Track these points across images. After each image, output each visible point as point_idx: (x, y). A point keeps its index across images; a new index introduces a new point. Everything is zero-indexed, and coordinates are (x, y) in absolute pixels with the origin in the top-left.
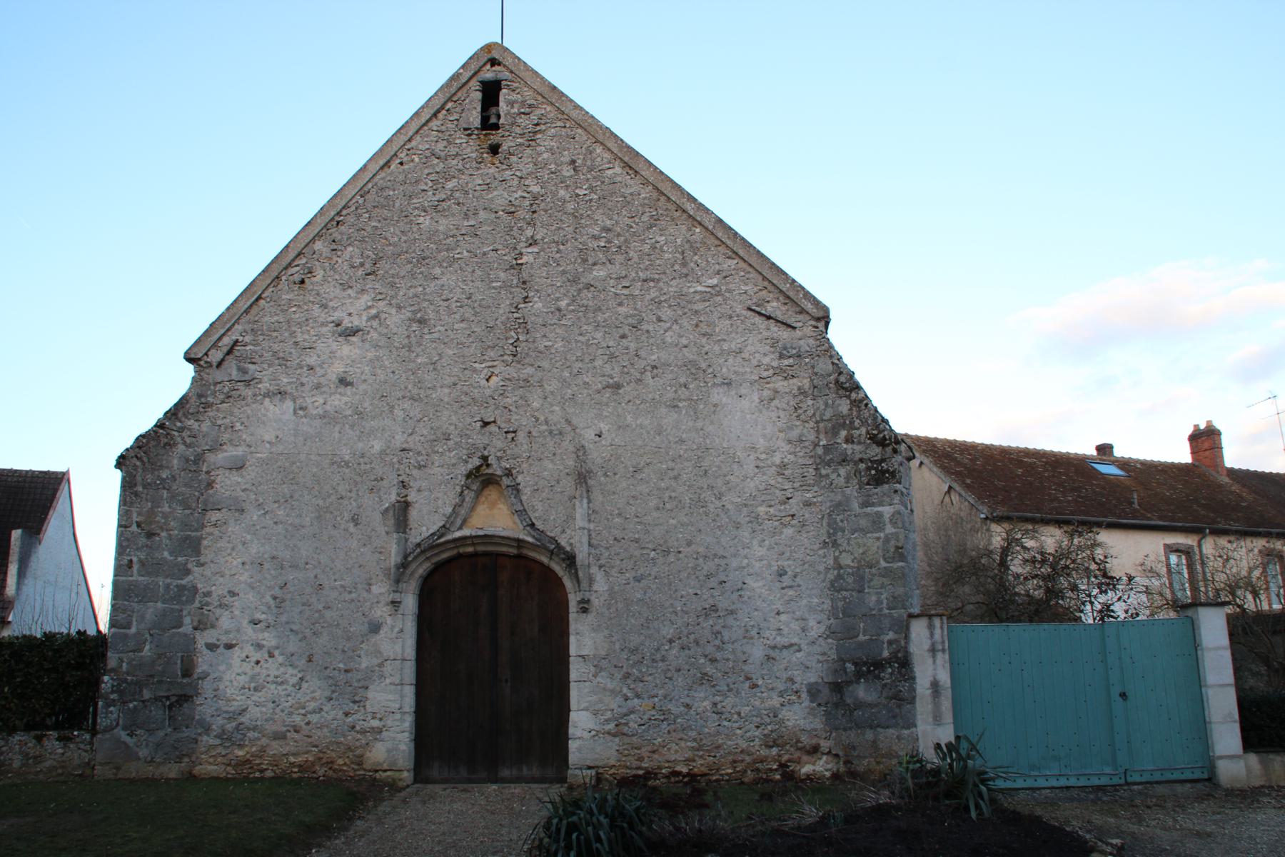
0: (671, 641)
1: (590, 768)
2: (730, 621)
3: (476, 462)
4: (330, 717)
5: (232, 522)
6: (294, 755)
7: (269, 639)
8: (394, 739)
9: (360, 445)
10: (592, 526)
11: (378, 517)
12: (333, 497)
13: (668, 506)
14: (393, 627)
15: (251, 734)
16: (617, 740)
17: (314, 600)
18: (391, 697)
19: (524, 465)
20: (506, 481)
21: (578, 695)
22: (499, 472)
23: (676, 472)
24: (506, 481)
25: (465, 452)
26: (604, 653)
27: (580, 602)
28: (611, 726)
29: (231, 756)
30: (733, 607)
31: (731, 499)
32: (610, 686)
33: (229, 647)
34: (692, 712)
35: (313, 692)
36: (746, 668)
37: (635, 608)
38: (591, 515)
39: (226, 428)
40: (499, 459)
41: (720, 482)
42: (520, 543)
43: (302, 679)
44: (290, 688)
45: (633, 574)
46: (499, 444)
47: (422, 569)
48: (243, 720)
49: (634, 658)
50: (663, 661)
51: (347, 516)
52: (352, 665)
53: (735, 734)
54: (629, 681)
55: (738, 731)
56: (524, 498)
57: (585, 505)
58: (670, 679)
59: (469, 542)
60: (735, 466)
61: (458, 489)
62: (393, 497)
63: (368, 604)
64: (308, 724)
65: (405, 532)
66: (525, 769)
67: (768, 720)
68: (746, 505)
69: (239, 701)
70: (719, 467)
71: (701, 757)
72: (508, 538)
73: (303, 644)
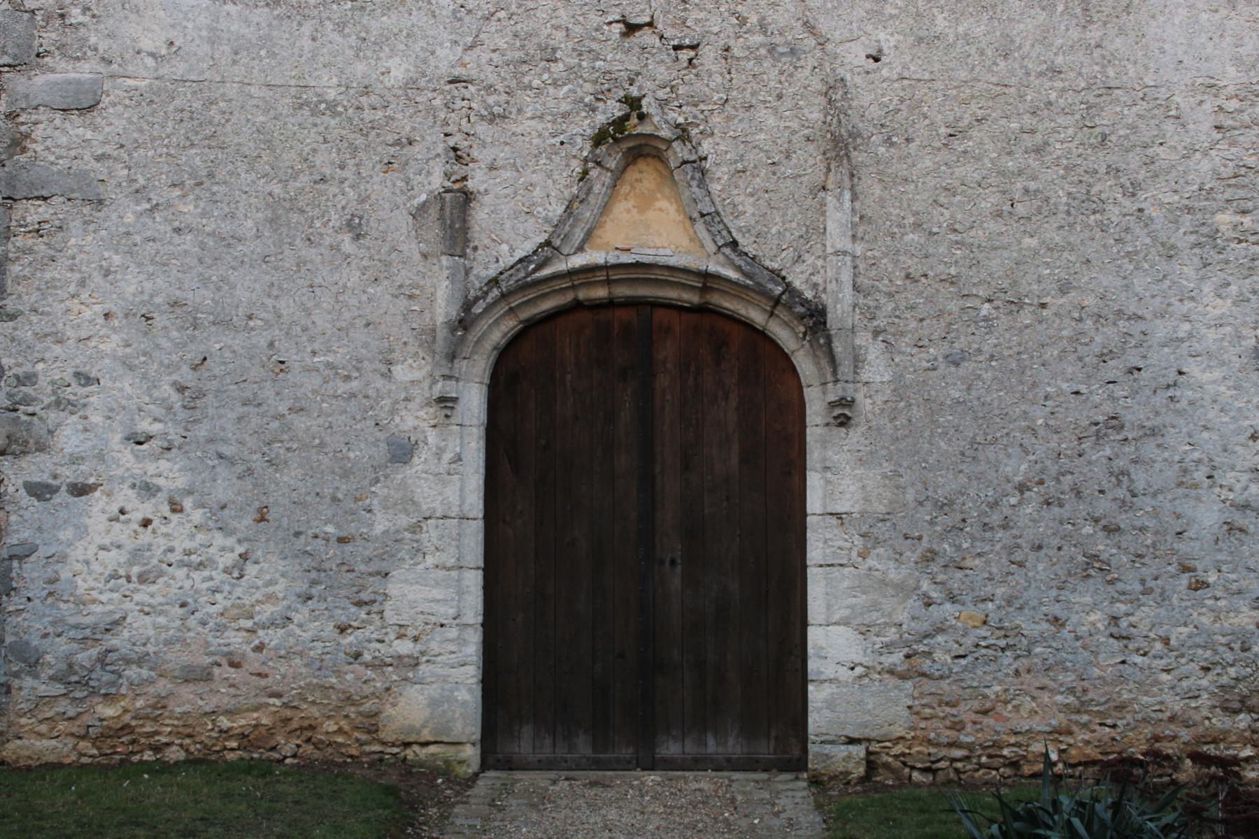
0: (1022, 488)
1: (851, 741)
2: (1149, 448)
3: (615, 109)
4: (307, 636)
5: (75, 225)
6: (229, 713)
7: (171, 474)
8: (445, 679)
9: (360, 68)
10: (859, 249)
11: (403, 222)
12: (304, 179)
13: (1020, 209)
14: (438, 455)
15: (132, 672)
16: (909, 685)
17: (268, 392)
18: (437, 593)
19: (716, 119)
20: (680, 151)
21: (823, 594)
22: (665, 133)
23: (1038, 138)
24: (680, 151)
25: (588, 87)
26: (882, 509)
27: (832, 405)
28: (896, 658)
29: (87, 719)
30: (1157, 421)
31: (1158, 197)
32: (893, 575)
33: (80, 490)
34: (1065, 632)
35: (270, 583)
36: (1182, 547)
37: (946, 418)
38: (860, 223)
39: (48, 18)
40: (663, 104)
41: (1134, 160)
42: (708, 280)
43: (244, 557)
44: (219, 576)
45: (945, 348)
46: (662, 74)
47: (498, 331)
48: (115, 642)
49: (948, 521)
50: (1005, 527)
51: (335, 219)
52: (351, 529)
53: (1157, 682)
54: (934, 568)
55: (1165, 677)
56: (715, 187)
57: (847, 204)
58: (1021, 565)
59: (601, 276)
60: (1169, 127)
61: (577, 167)
62: (437, 181)
63: (387, 402)
64: (259, 648)
65: (463, 255)
66: (711, 742)
67: (1229, 657)
68: (1189, 210)
69: (106, 604)
70: (1133, 128)
71: (1085, 726)
72: (685, 271)
73: (248, 484)
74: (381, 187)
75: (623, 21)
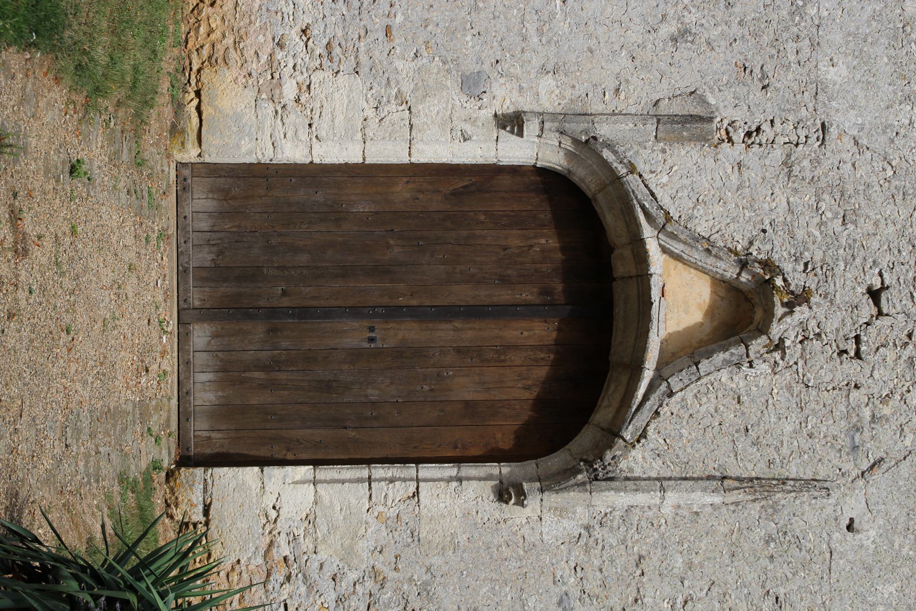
51: (691, 18)
54: (369, 584)
74: (720, 62)
75: (884, 288)
